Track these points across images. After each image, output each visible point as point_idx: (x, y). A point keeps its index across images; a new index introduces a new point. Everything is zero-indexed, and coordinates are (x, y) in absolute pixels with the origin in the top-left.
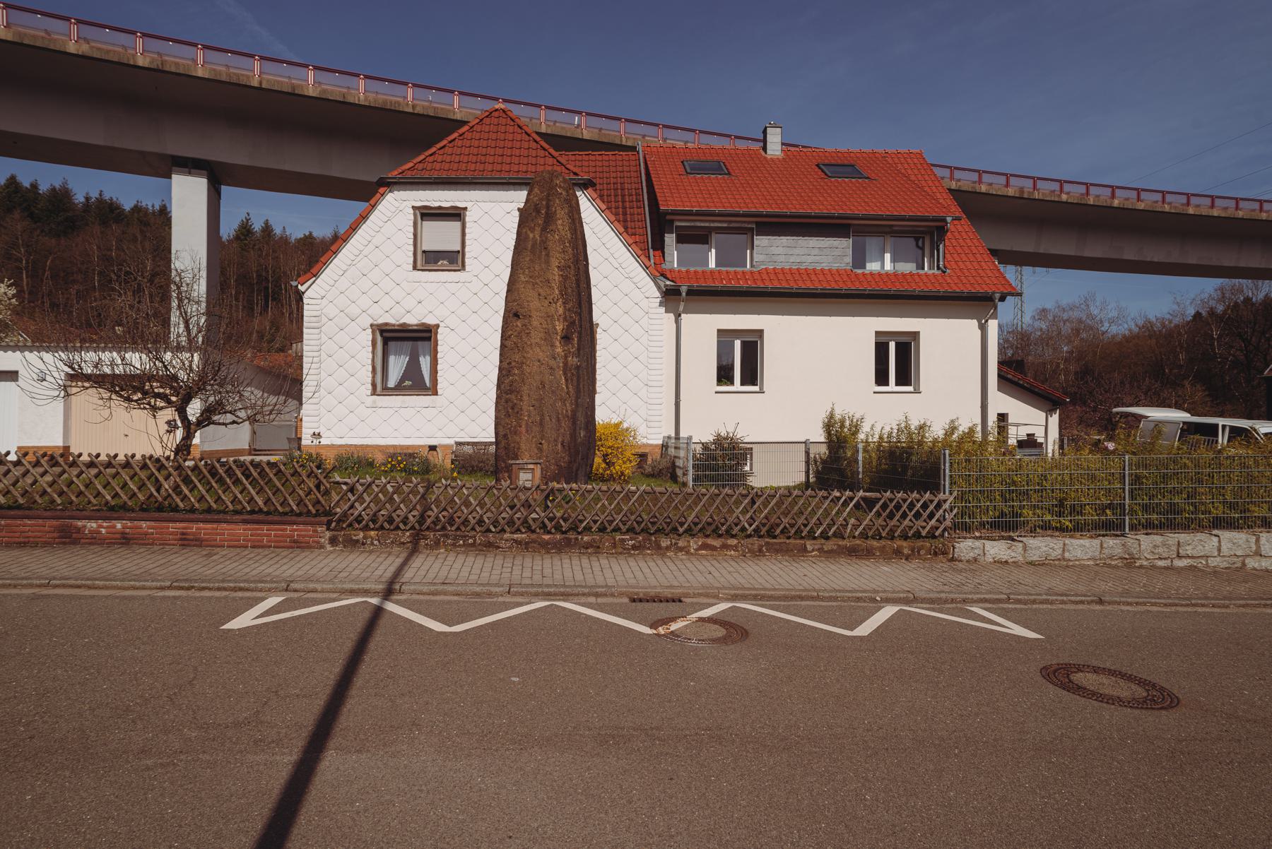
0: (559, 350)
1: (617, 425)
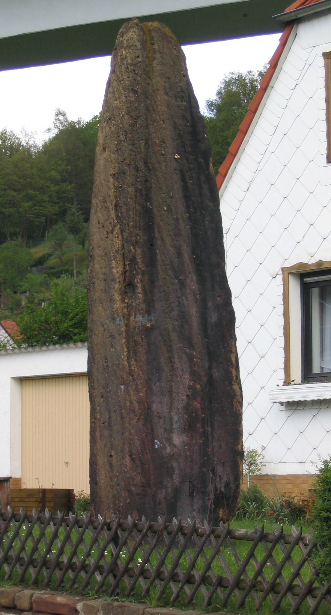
0: (118, 305)
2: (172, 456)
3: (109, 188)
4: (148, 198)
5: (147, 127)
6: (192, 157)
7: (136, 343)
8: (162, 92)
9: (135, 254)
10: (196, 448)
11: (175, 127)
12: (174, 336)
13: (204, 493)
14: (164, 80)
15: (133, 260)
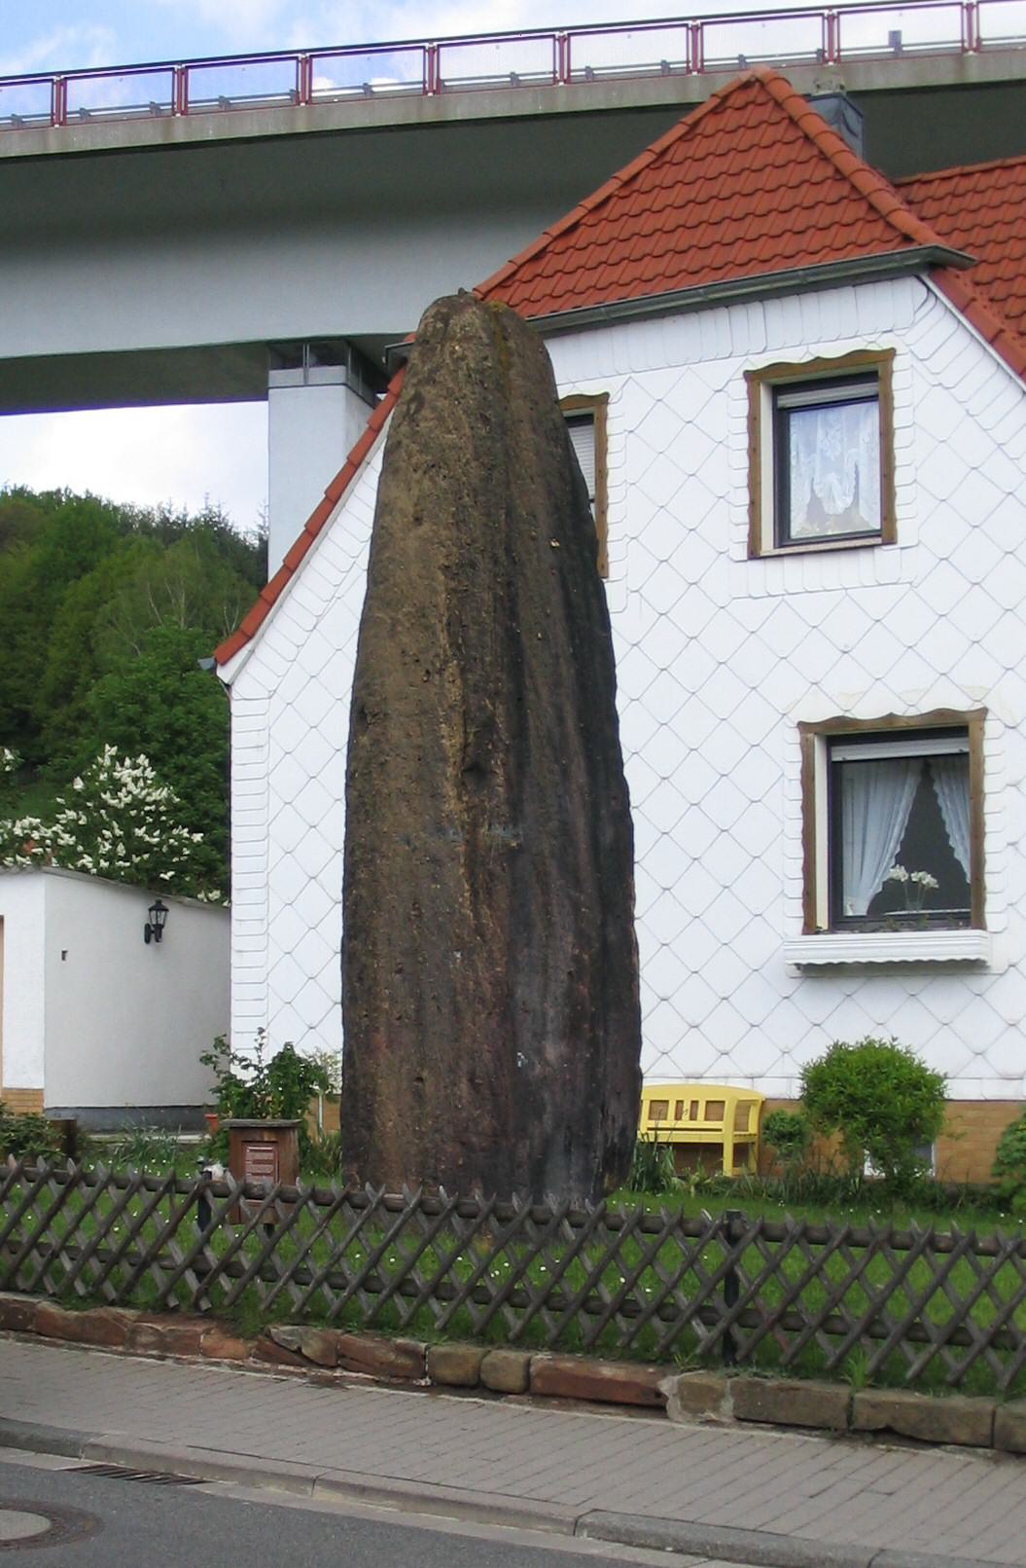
0: (451, 806)
1: (939, 1079)
3: (435, 592)
4: (513, 615)
5: (508, 485)
7: (491, 874)
8: (526, 426)
9: (494, 715)
10: (581, 1066)
12: (552, 867)
13: (588, 1147)
15: (488, 726)
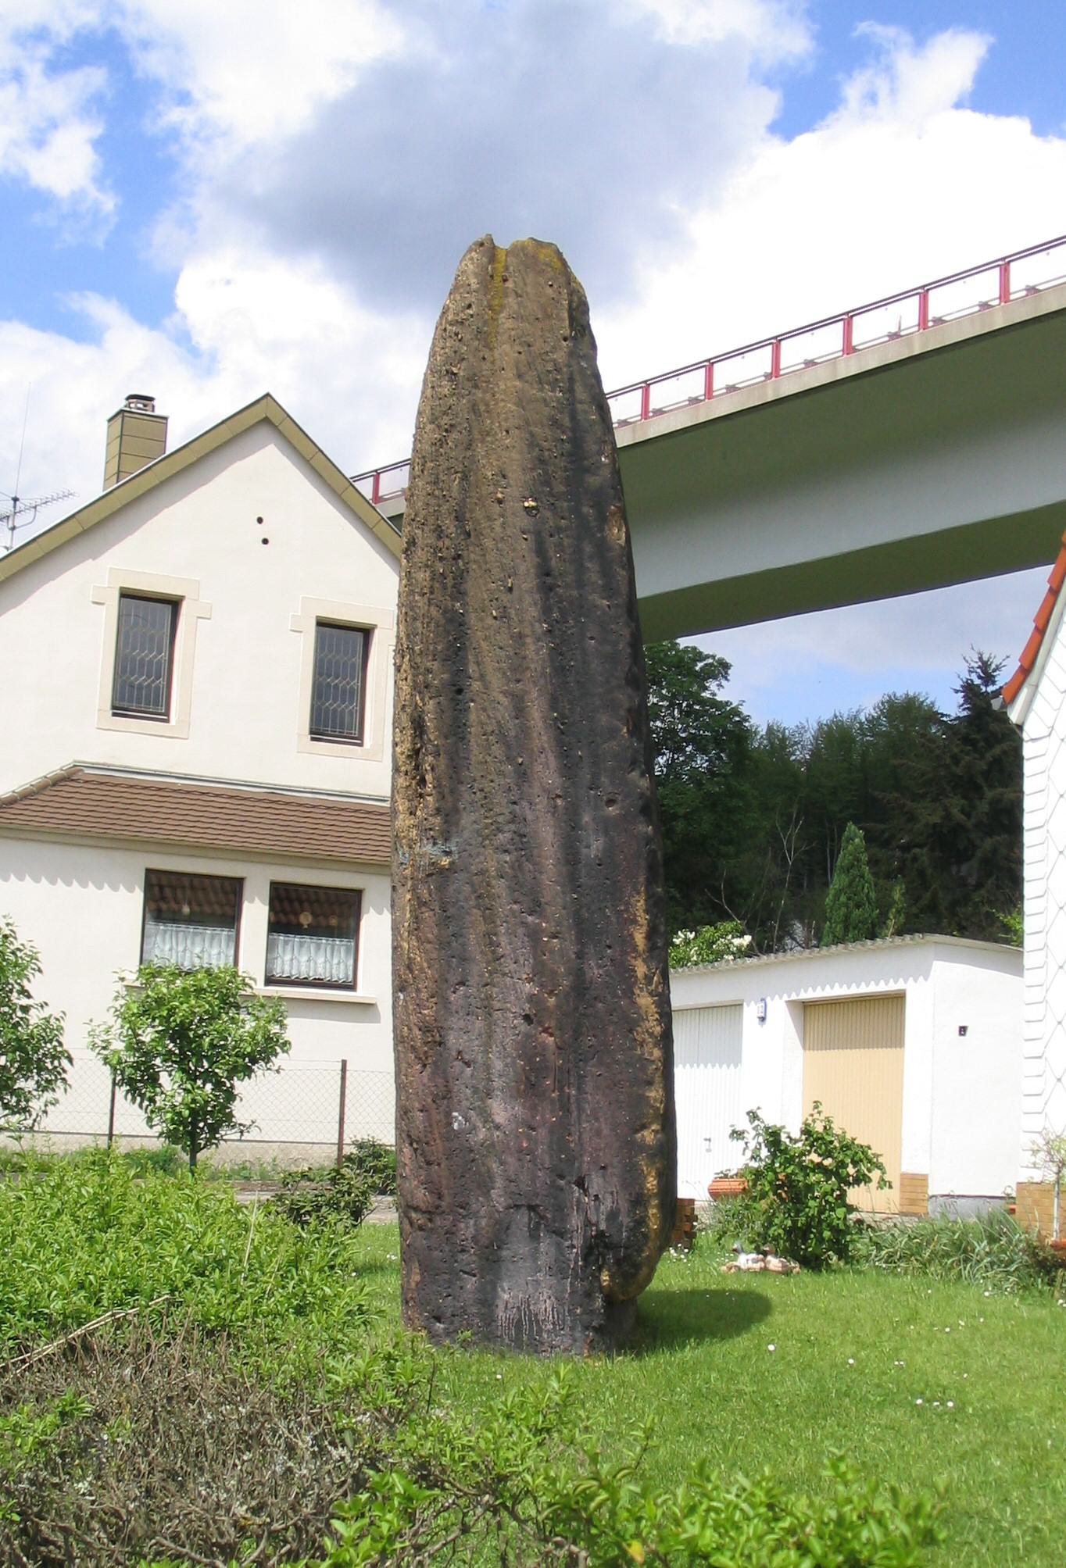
2: (490, 1147)
4: (459, 593)
6: (565, 504)
8: (510, 373)
10: (542, 1133)
11: (532, 443)
12: (500, 887)
14: (518, 348)
